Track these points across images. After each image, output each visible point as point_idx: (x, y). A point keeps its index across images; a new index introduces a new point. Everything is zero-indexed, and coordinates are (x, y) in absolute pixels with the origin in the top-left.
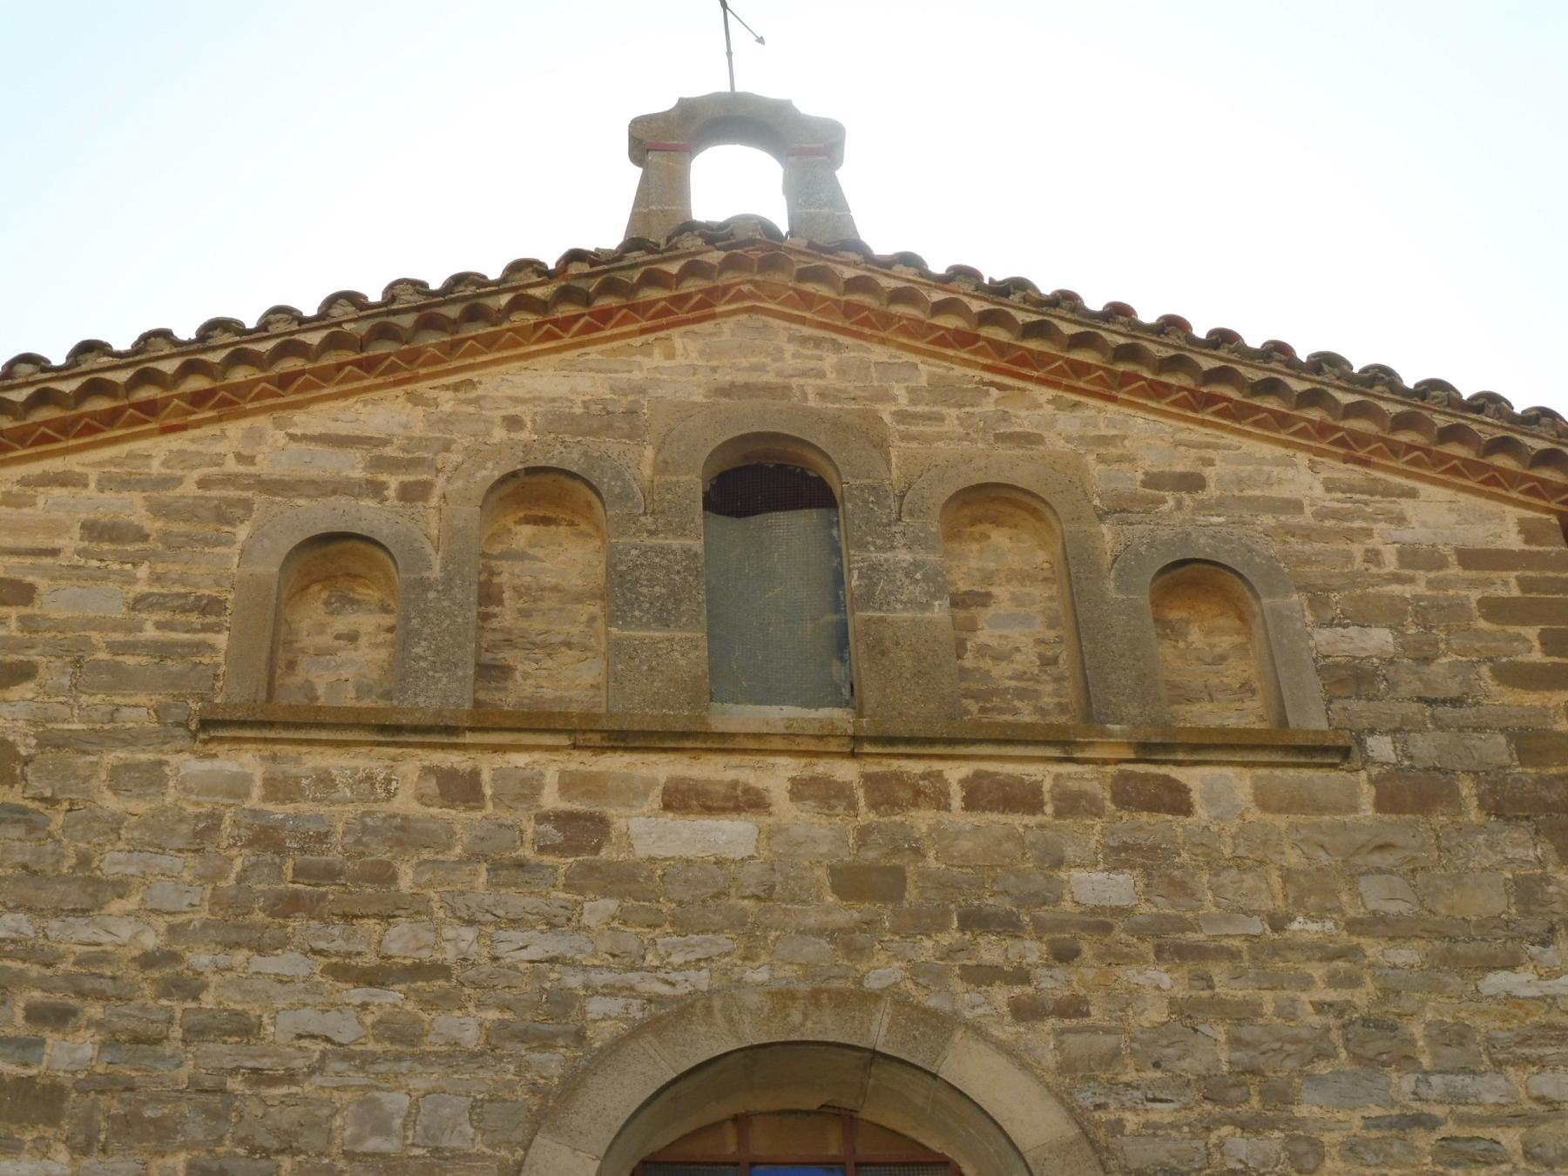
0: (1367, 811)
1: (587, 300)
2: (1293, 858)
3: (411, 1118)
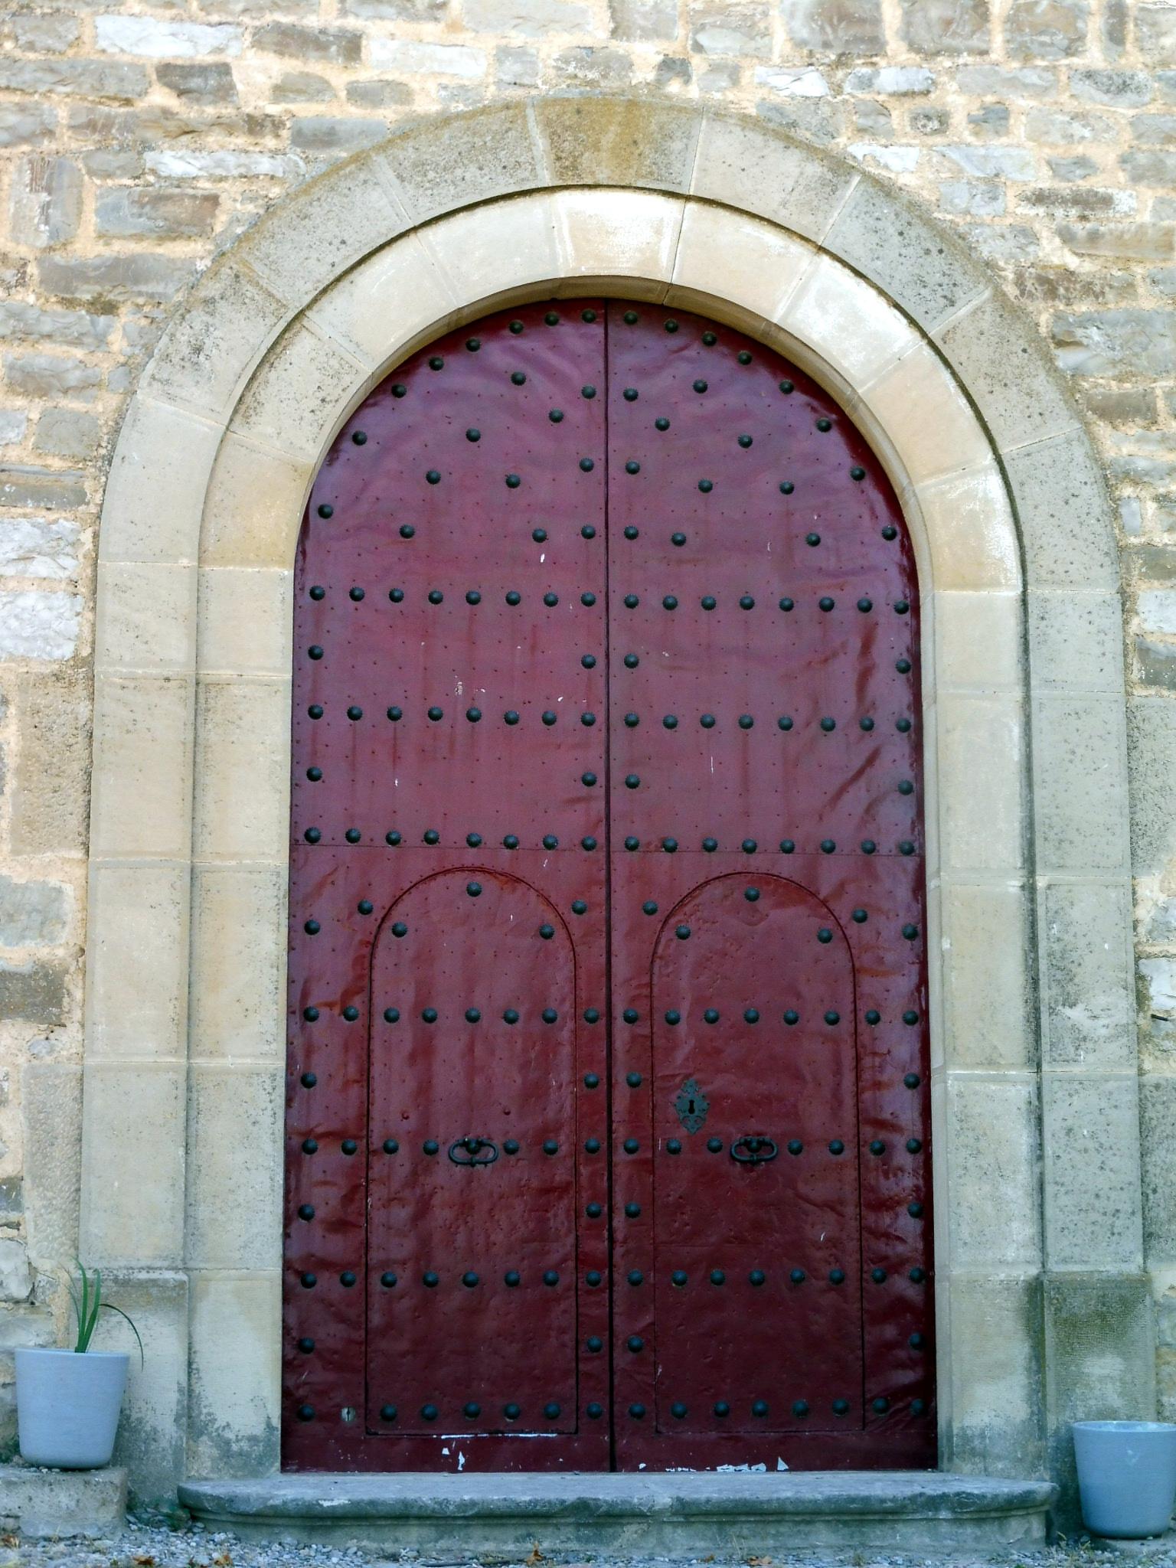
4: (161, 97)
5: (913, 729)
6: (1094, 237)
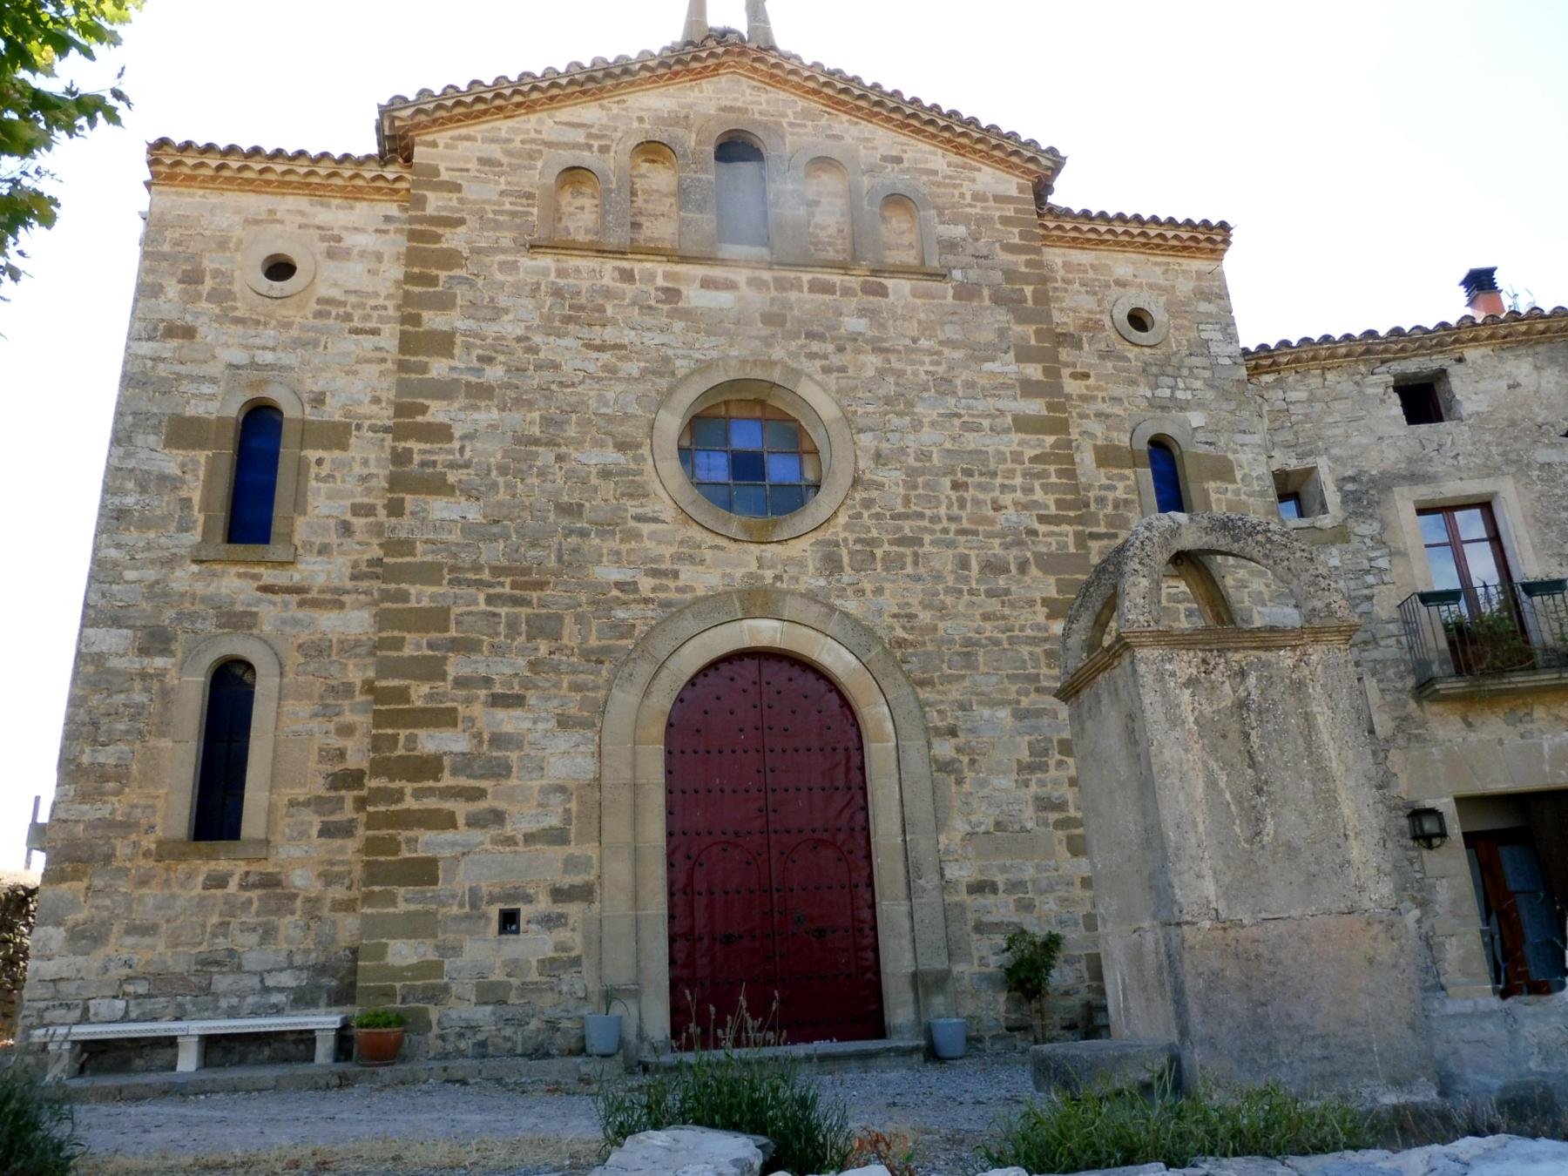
0: (950, 299)
1: (670, 67)
2: (922, 316)
3: (616, 401)
4: (615, 593)
5: (864, 789)
6: (912, 628)
